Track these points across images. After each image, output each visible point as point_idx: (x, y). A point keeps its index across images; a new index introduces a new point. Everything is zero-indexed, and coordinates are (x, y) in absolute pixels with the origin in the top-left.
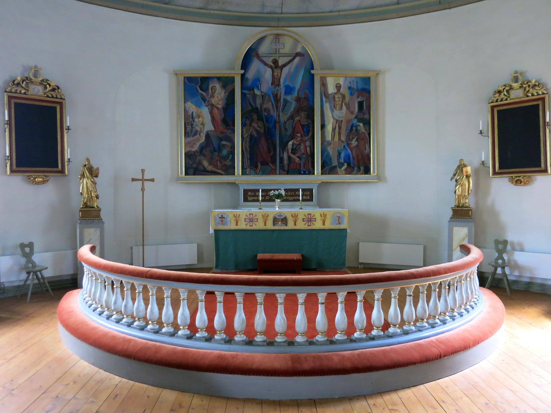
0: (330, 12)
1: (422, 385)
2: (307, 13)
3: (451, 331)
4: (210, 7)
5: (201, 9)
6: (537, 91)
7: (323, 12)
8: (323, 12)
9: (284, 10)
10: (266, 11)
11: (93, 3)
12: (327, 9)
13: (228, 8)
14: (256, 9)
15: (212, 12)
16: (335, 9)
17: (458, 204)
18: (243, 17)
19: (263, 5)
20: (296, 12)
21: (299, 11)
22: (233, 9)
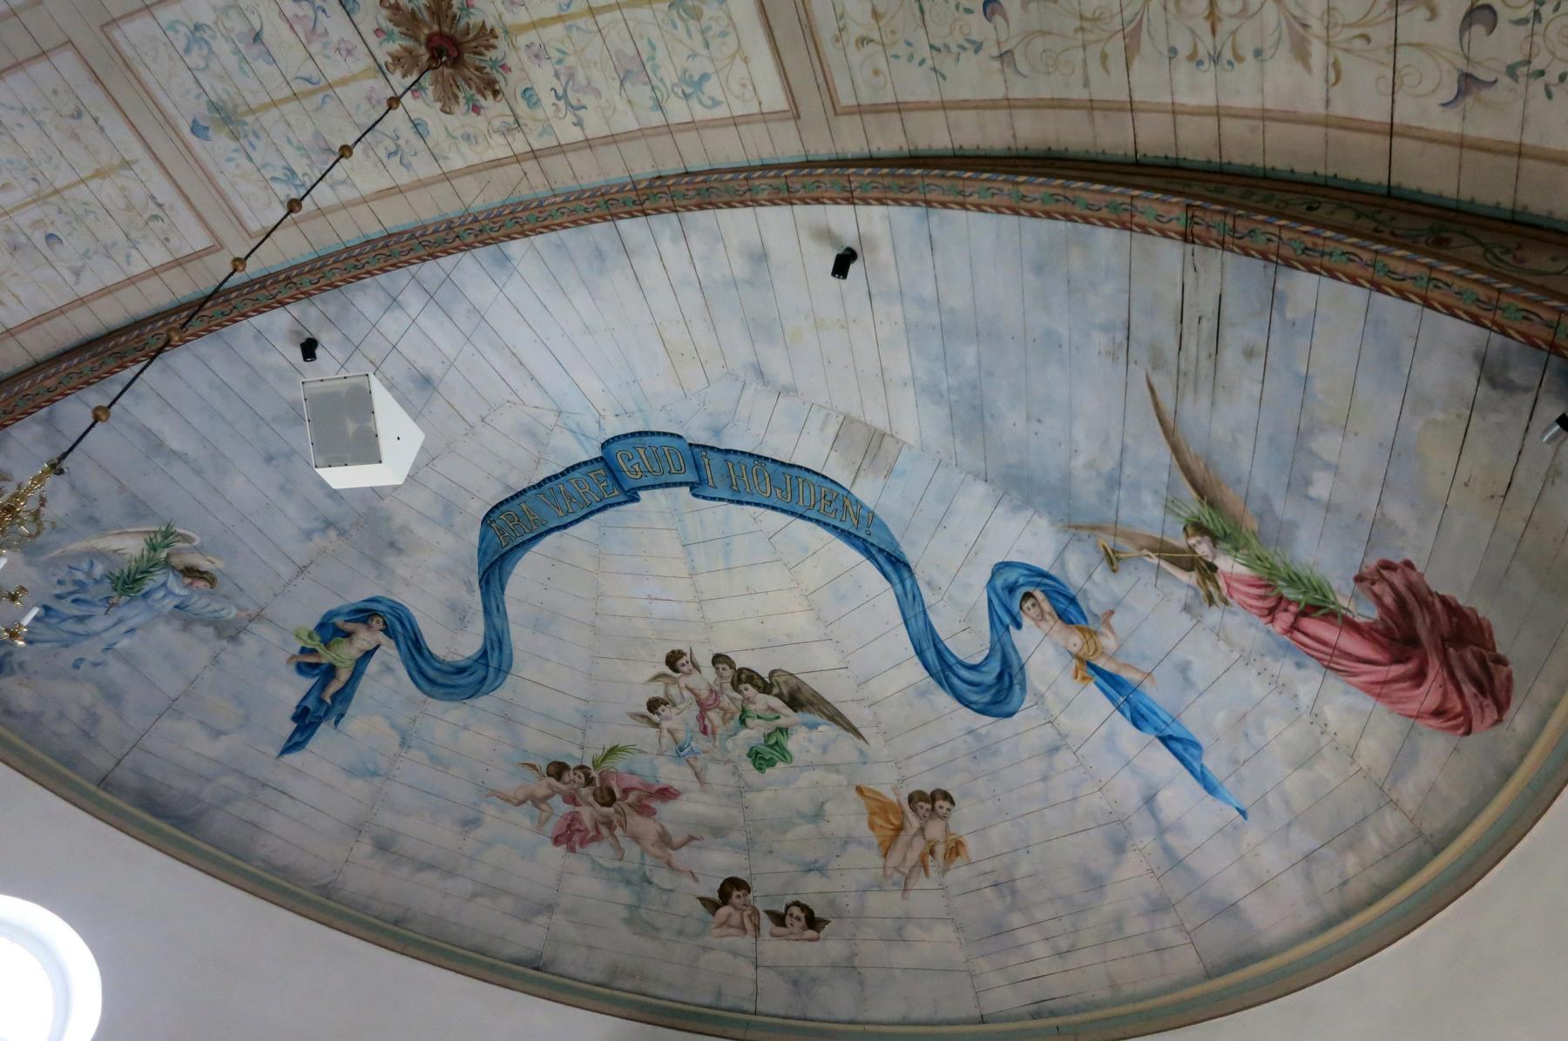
0: (851, 1022)
1: (902, 621)
2: (805, 1019)
3: (931, 625)
4: (618, 984)
5: (598, 985)
6: (182, 53)
7: (837, 1022)
8: (837, 1022)
9: (761, 1008)
10: (724, 1004)
11: (1247, 1004)
12: (845, 1017)
13: (651, 990)
14: (707, 999)
15: (616, 993)
16: (861, 1018)
17: (174, 267)
18: (690, 1013)
19: (719, 993)
20: (783, 1013)
21: (790, 1013)
22: (661, 993)
